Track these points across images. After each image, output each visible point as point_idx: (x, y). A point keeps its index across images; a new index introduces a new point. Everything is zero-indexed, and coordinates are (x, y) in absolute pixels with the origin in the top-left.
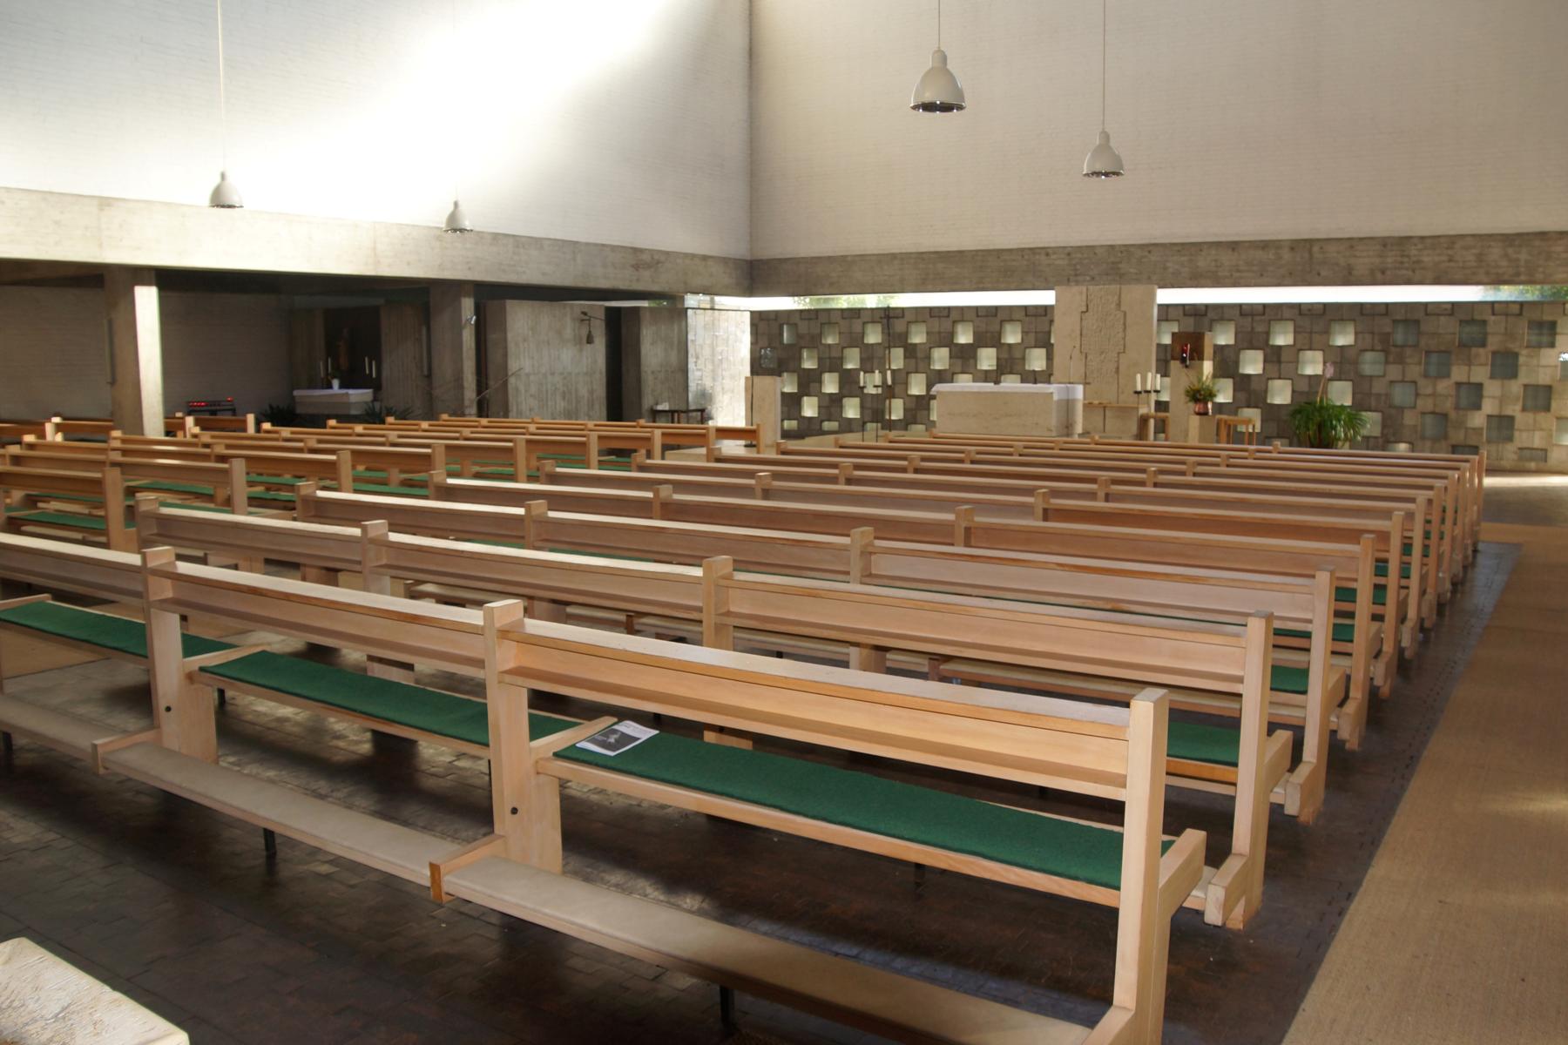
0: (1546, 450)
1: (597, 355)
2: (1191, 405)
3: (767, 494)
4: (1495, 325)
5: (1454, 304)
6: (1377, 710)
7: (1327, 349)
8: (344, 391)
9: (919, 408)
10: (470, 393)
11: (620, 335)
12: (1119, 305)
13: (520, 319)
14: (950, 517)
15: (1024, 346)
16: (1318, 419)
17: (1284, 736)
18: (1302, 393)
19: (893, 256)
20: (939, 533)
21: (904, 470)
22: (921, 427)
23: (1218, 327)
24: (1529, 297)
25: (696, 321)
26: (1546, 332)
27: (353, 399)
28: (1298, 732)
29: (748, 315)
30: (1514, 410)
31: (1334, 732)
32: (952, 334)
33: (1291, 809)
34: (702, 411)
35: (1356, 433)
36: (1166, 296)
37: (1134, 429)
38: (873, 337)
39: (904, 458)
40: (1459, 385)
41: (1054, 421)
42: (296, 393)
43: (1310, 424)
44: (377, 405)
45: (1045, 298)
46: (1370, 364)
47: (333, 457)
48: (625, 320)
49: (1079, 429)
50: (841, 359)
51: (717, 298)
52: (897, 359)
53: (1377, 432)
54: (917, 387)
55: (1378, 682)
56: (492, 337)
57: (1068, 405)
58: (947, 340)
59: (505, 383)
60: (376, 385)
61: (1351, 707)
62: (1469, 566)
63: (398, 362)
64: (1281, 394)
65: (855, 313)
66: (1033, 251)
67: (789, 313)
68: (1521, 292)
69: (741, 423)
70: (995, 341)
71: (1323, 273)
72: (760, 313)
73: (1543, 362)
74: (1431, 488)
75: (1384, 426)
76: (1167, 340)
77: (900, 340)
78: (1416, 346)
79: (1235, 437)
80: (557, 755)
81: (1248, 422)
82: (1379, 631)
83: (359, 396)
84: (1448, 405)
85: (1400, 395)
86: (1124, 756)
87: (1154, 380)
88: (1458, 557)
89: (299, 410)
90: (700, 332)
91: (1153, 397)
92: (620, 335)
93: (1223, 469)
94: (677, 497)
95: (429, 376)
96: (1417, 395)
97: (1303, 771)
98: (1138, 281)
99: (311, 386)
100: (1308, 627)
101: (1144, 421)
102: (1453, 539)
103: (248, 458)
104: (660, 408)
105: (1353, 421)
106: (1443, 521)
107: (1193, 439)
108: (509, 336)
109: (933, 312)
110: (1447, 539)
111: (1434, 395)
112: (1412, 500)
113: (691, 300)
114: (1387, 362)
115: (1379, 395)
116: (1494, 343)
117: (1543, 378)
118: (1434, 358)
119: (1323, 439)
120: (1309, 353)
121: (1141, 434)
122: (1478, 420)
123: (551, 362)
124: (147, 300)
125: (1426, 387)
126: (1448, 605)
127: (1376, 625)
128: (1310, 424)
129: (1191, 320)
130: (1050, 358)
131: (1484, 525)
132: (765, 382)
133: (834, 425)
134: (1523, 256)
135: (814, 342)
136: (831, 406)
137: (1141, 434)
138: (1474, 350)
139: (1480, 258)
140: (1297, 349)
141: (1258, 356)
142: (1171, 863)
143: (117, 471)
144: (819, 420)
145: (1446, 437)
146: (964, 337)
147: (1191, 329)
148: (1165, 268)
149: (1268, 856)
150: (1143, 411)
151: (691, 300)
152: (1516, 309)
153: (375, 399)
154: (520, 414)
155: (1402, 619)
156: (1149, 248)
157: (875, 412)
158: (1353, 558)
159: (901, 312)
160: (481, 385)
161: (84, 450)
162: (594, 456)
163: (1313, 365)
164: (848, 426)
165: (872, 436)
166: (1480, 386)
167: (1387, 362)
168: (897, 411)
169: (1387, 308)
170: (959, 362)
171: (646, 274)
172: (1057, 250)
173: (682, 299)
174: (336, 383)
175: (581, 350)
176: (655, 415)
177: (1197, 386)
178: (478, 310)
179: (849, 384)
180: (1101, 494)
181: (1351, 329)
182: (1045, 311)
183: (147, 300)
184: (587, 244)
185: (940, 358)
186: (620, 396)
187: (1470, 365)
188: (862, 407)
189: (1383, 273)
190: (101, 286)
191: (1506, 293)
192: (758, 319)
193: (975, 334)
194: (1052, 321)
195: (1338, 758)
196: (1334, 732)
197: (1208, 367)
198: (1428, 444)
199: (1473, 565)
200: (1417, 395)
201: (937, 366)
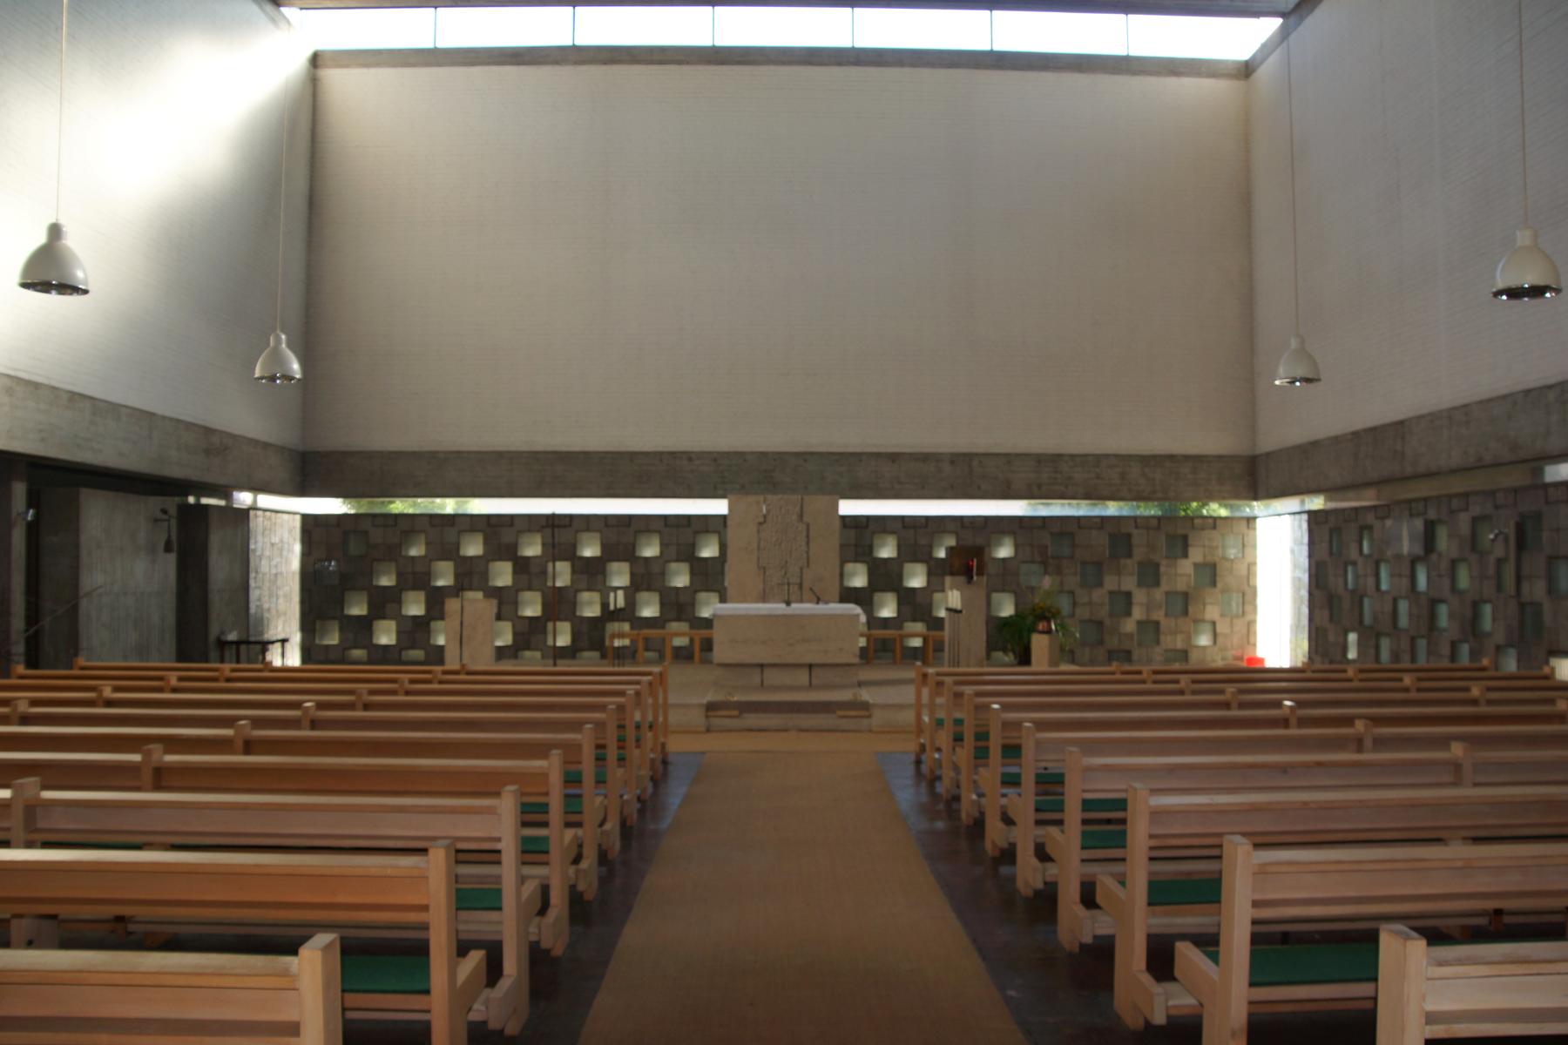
4: (1139, 538)
12: (801, 517)
15: (663, 559)
17: (476, 957)
28: (545, 890)
29: (298, 518)
30: (1158, 615)
38: (473, 548)
39: (350, 692)
40: (1111, 593)
54: (415, 607)
66: (673, 455)
73: (1180, 571)
74: (622, 693)
84: (1103, 613)
94: (169, 758)
100: (498, 846)
108: (83, 538)
109: (607, 520)
111: (1090, 603)
116: (1139, 553)
117: (1181, 585)
122: (1129, 626)
129: (852, 533)
133: (418, 654)
135: (392, 552)
138: (1122, 561)
145: (1101, 642)
146: (590, 551)
152: (1155, 522)
156: (805, 456)
159: (510, 520)
166: (1128, 595)
178: (33, 500)
181: (538, 539)
192: (311, 524)
193: (604, 547)
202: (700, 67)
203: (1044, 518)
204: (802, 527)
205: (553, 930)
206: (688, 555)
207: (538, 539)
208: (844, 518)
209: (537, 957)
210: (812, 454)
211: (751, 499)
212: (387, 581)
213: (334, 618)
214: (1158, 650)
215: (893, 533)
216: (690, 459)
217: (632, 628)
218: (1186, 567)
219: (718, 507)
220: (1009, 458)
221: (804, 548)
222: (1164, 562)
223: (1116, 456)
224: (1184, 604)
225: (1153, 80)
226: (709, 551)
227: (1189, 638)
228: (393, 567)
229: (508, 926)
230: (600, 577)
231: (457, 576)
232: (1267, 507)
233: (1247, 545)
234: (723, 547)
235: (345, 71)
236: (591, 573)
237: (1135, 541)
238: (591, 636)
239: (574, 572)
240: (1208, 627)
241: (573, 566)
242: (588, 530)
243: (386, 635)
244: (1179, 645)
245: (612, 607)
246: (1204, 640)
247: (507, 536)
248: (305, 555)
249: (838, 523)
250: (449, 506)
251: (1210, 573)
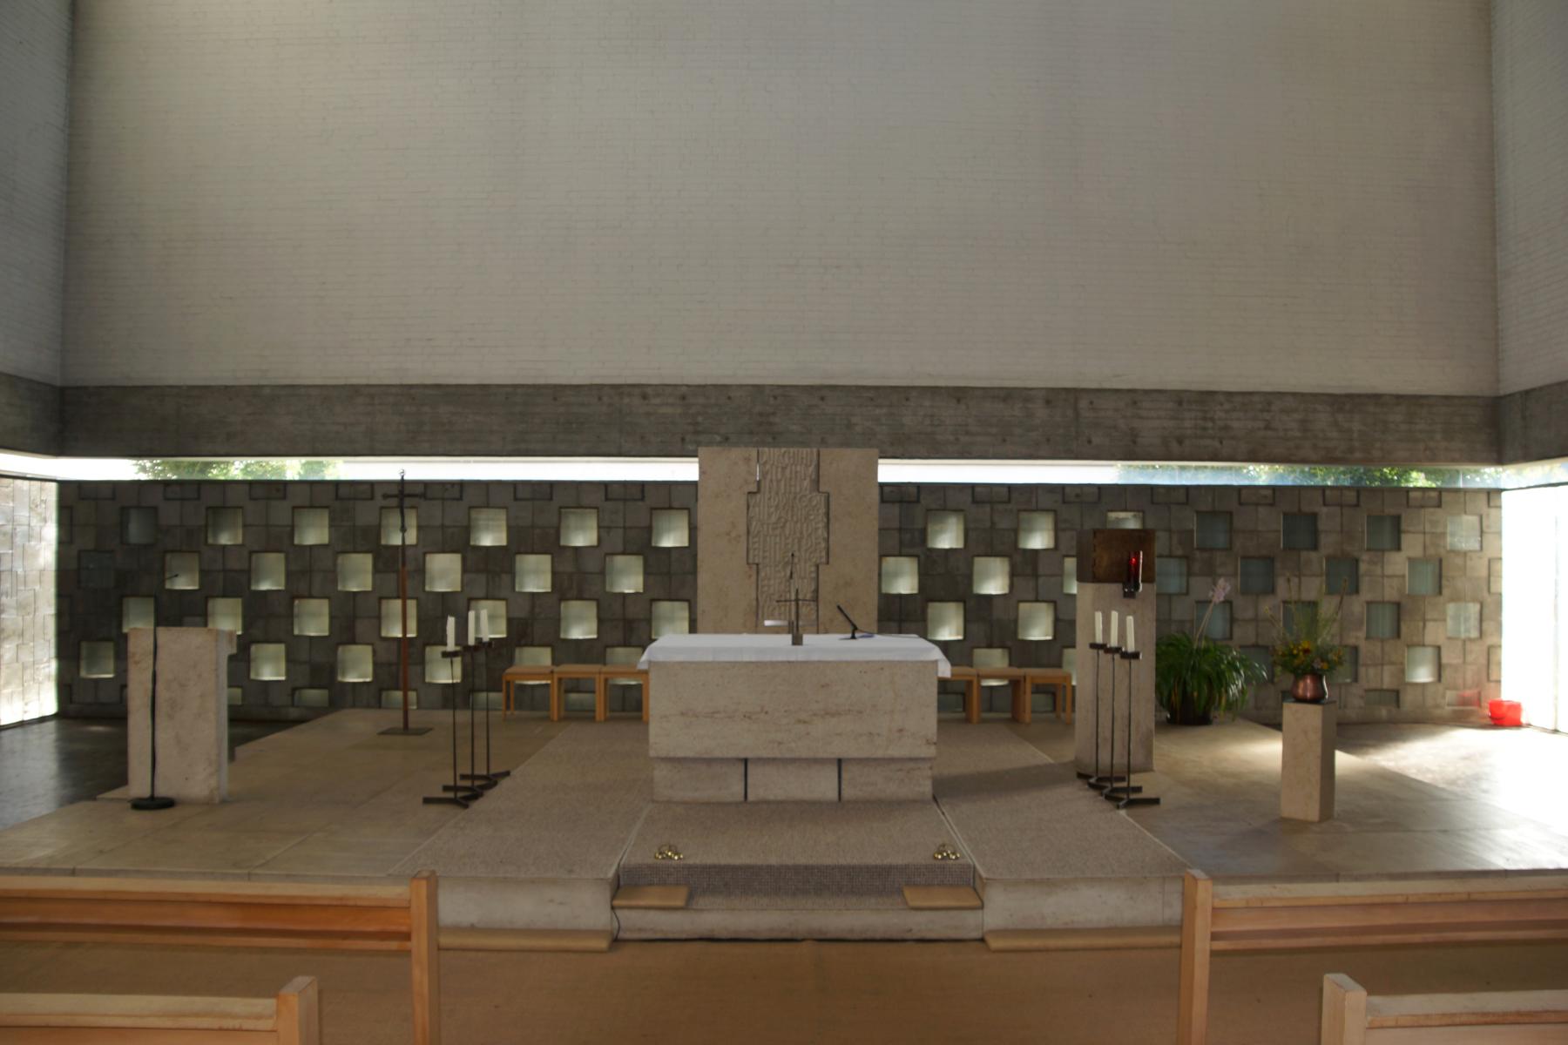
0: (1397, 693)
4: (1328, 520)
15: (602, 550)
32: (467, 530)
50: (248, 574)
58: (458, 541)
70: (550, 543)
71: (1096, 440)
73: (1389, 570)
77: (369, 540)
78: (1229, 549)
111: (1256, 620)
114: (1189, 574)
115: (1182, 622)
116: (1328, 542)
117: (1390, 594)
135: (193, 541)
136: (317, 666)
138: (1304, 554)
144: (291, 689)
146: (490, 537)
148: (849, 426)
159: (369, 488)
167: (1189, 574)
168: (358, 669)
170: (482, 579)
172: (662, 389)
181: (500, 519)
188: (290, 660)
189: (1180, 442)
192: (72, 496)
203: (1187, 488)
204: (819, 499)
206: (642, 545)
207: (500, 519)
208: (883, 485)
211: (736, 453)
212: (184, 583)
213: (108, 639)
214: (1356, 690)
215: (956, 511)
216: (645, 397)
217: (555, 662)
218: (1397, 563)
219: (684, 470)
220: (1134, 397)
221: (821, 532)
222: (1365, 557)
223: (1294, 394)
224: (1401, 617)
226: (672, 538)
227: (1402, 672)
228: (193, 561)
230: (506, 578)
231: (289, 575)
232: (1519, 473)
233: (1487, 531)
234: (693, 531)
236: (491, 571)
237: (1322, 525)
238: (487, 664)
239: (465, 570)
240: (1429, 653)
241: (464, 560)
244: (1387, 682)
245: (471, 641)
246: (1423, 675)
247: (365, 515)
248: (62, 542)
249: (875, 495)
250: (292, 468)
251: (1441, 572)
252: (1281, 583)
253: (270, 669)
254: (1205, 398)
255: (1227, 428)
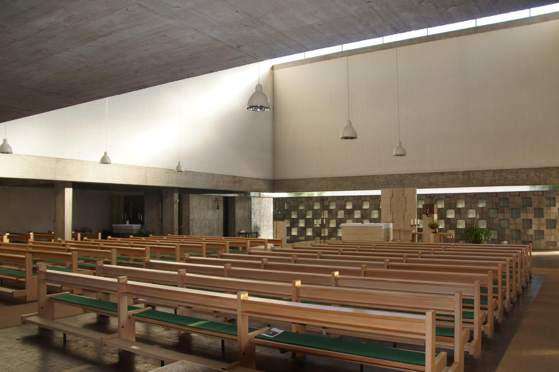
1: (220, 213)
2: (431, 230)
3: (296, 262)
4: (535, 199)
5: (519, 192)
6: (497, 326)
7: (477, 209)
8: (131, 225)
9: (333, 232)
10: (176, 226)
11: (228, 206)
12: (403, 195)
13: (194, 201)
14: (360, 268)
15: (370, 210)
16: (475, 233)
18: (469, 224)
19: (324, 179)
20: (357, 273)
21: (337, 254)
22: (334, 238)
23: (438, 202)
24: (545, 189)
25: (254, 201)
26: (552, 201)
27: (134, 228)
28: (472, 332)
30: (543, 228)
31: (483, 332)
32: (345, 206)
33: (471, 353)
34: (257, 233)
35: (489, 238)
36: (420, 191)
37: (411, 238)
38: (317, 207)
40: (523, 220)
41: (383, 236)
42: (113, 225)
43: (472, 235)
44: (143, 230)
45: (378, 192)
46: (492, 214)
47: (144, 249)
48: (230, 202)
49: (391, 238)
50: (306, 215)
51: (262, 193)
52: (326, 215)
53: (496, 237)
54: (333, 224)
55: (497, 318)
56: (184, 207)
57: (388, 230)
58: (343, 208)
59: (189, 223)
60: (142, 223)
61: (488, 325)
62: (528, 282)
63: (150, 216)
64: (461, 225)
65: (311, 198)
67: (287, 198)
68: (543, 187)
69: (271, 237)
72: (277, 198)
73: (552, 211)
75: (498, 235)
76: (421, 206)
78: (508, 207)
79: (446, 240)
80: (256, 337)
81: (450, 235)
82: (495, 302)
83: (136, 227)
84: (520, 227)
85: (504, 224)
86: (424, 328)
87: (417, 221)
88: (524, 279)
89: (114, 232)
90: (256, 205)
91: (417, 227)
92: (228, 206)
93: (443, 252)
95: (162, 220)
96: (509, 224)
97: (474, 342)
98: (410, 186)
99: (118, 223)
100: (453, 314)
101: (414, 235)
102: (521, 273)
103: (117, 249)
104: (242, 232)
105: (487, 234)
106: (517, 267)
107: (432, 242)
108: (190, 206)
109: (338, 198)
110: (519, 273)
111: (515, 224)
112: (505, 260)
113: (252, 194)
114: (498, 213)
115: (496, 224)
116: (534, 205)
117: (553, 217)
118: (514, 211)
119: (477, 241)
120: (470, 210)
121: (413, 240)
122: (531, 232)
123: (204, 215)
124: (69, 193)
125: (512, 221)
126: (521, 295)
127: (495, 299)
128: (472, 235)
129: (429, 199)
130: (380, 213)
131: (533, 269)
132: (280, 223)
133: (303, 238)
134: (542, 175)
135: (296, 208)
136: (302, 231)
137: (413, 240)
138: (528, 208)
139: (527, 176)
140: (466, 209)
141: (453, 211)
142: (438, 360)
143: (76, 253)
146: (349, 207)
147: (429, 203)
148: (419, 182)
149: (465, 367)
150: (414, 232)
151: (252, 194)
152: (541, 193)
153: (142, 228)
154: (193, 234)
155: (504, 298)
157: (317, 233)
158: (485, 278)
160: (180, 224)
161: (17, 247)
162: (228, 249)
163: (472, 214)
164: (308, 238)
165: (318, 242)
166: (531, 220)
167: (498, 213)
168: (326, 233)
169: (497, 194)
171: (237, 185)
172: (381, 176)
173: (249, 194)
174: (128, 222)
175: (215, 212)
176: (240, 234)
177: (432, 223)
178: (180, 197)
179: (309, 223)
180: (405, 261)
182: (378, 197)
183: (69, 193)
184: (217, 175)
185: (341, 214)
186: (228, 228)
187: (527, 213)
188: (313, 231)
189: (495, 182)
190: (51, 188)
191: (537, 188)
192: (276, 200)
194: (380, 201)
195: (484, 339)
196: (483, 332)
197: (436, 216)
198: (514, 241)
199: (530, 282)
200: (509, 224)
201: (339, 217)
202: (377, 52)
205: (473, 349)
209: (468, 358)
210: (416, 174)
222: (545, 208)
223: (524, 169)
225: (537, 25)
229: (458, 345)
231: (313, 215)
235: (280, 70)
242: (366, 201)
243: (309, 233)
250: (316, 194)
252: (522, 215)
253: (294, 232)
254: (501, 171)
255: (506, 178)
